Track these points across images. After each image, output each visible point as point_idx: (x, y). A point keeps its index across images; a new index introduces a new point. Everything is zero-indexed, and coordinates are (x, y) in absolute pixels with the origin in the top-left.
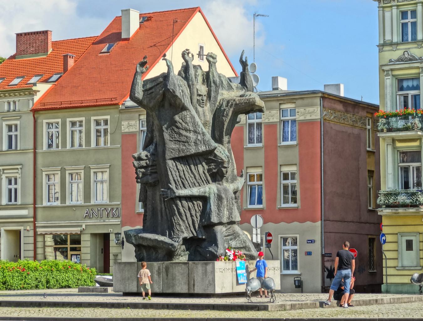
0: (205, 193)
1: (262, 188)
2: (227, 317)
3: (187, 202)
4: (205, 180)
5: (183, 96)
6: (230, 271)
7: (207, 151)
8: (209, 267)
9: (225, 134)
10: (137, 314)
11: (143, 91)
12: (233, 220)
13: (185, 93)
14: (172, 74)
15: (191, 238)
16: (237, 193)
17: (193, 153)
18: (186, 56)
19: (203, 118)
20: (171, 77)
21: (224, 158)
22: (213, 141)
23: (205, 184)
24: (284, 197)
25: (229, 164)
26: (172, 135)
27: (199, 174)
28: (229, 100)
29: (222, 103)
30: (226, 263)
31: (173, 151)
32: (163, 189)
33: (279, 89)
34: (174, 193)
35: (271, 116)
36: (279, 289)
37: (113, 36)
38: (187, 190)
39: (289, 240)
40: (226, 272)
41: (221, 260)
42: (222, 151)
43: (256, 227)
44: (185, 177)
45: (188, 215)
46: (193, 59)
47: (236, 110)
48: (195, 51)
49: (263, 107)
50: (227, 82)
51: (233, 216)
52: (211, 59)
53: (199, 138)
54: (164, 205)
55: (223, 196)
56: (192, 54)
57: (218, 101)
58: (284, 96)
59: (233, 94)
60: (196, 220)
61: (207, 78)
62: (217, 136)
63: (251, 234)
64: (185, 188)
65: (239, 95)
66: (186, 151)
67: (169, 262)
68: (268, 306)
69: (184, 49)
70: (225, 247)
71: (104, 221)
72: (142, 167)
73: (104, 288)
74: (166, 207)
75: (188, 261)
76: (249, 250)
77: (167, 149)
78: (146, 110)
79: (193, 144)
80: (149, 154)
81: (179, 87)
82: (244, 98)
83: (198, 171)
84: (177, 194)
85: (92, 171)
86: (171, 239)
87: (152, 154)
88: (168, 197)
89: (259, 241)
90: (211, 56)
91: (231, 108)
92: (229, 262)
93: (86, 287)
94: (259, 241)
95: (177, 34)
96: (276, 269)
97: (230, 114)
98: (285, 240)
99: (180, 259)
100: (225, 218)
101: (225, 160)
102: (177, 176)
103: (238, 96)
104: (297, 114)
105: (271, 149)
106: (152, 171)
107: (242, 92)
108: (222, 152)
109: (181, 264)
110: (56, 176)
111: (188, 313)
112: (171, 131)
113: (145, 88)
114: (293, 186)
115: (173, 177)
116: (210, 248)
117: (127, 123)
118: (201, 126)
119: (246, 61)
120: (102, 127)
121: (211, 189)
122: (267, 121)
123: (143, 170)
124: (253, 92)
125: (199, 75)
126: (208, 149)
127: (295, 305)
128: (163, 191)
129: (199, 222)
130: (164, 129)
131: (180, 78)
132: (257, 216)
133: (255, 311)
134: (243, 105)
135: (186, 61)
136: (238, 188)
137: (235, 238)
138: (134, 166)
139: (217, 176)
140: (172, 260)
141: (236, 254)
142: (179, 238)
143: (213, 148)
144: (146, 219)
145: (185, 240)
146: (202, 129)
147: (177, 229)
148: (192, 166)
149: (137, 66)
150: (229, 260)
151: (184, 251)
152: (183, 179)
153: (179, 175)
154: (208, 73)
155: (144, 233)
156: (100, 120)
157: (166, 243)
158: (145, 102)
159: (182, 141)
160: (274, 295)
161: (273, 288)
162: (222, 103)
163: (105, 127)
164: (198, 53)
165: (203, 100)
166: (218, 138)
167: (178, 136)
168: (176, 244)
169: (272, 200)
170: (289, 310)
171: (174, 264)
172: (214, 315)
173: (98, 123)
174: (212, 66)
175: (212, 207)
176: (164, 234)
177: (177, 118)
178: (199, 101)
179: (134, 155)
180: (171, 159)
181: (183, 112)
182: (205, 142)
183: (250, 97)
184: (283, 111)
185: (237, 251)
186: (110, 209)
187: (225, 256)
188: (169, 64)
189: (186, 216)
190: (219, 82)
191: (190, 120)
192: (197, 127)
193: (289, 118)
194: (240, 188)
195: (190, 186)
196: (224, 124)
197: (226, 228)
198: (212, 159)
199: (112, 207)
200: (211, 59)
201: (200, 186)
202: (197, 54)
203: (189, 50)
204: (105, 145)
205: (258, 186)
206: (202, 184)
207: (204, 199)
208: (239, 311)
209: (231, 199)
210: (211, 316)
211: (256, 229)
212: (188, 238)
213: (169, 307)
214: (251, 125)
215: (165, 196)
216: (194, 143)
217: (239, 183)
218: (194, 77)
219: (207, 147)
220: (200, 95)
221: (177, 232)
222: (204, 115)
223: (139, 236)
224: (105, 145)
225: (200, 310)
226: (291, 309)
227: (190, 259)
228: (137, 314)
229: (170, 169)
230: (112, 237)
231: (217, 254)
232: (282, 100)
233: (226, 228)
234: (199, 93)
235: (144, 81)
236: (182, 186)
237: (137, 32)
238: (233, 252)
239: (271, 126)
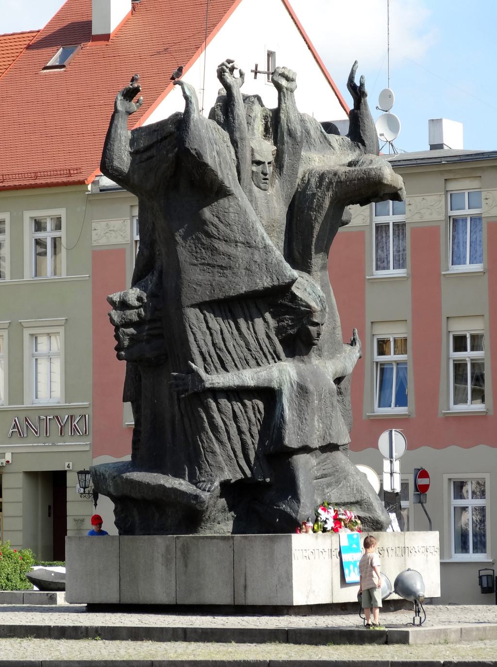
0: (271, 381)
1: (406, 368)
2: (315, 658)
3: (230, 401)
4: (269, 352)
5: (220, 164)
6: (327, 555)
7: (274, 287)
8: (279, 546)
9: (315, 248)
10: (114, 651)
11: (131, 153)
12: (334, 441)
13: (225, 158)
14: (195, 115)
15: (239, 482)
16: (343, 382)
17: (242, 291)
18: (227, 74)
19: (264, 214)
20: (192, 124)
21: (313, 304)
22: (288, 266)
23: (271, 361)
24: (455, 388)
25: (323, 316)
26: (196, 252)
27: (257, 339)
28: (323, 174)
29: (309, 180)
30: (317, 538)
31: (198, 288)
32: (175, 374)
33: (445, 146)
34: (201, 381)
35: (421, 207)
36: (437, 594)
37: (73, 32)
38: (229, 374)
39: (469, 488)
40: (317, 556)
41: (306, 532)
42: (309, 288)
43: (391, 456)
44: (225, 345)
45: (233, 430)
46: (243, 82)
47: (339, 194)
48: (244, 64)
49: (401, 189)
50: (319, 133)
51: (333, 434)
52: (282, 82)
53: (257, 257)
54: (179, 406)
55: (311, 387)
56: (240, 71)
57: (300, 175)
58: (454, 162)
59: (330, 159)
60: (249, 441)
61: (275, 125)
62: (297, 253)
63: (379, 472)
64: (227, 370)
65: (347, 162)
66: (227, 287)
67: (191, 535)
68: (407, 633)
69: (224, 60)
70: (316, 502)
71: (54, 445)
72: (128, 324)
73: (47, 594)
74: (183, 412)
75: (232, 533)
76: (369, 508)
77: (185, 282)
78: (137, 196)
79: (243, 271)
80: (144, 296)
81: (212, 146)
82: (357, 168)
83: (255, 333)
84: (207, 385)
85: (26, 333)
86: (195, 484)
87: (151, 296)
88: (187, 390)
89: (398, 489)
90: (283, 75)
91: (328, 190)
92: (325, 535)
93: (9, 591)
94: (398, 489)
95: (215, 25)
96: (431, 550)
97: (327, 203)
98: (459, 487)
99: (216, 529)
100: (315, 436)
101: (316, 307)
102: (206, 345)
103: (344, 165)
104: (484, 202)
105: (427, 284)
106: (151, 332)
107: (351, 157)
108: (308, 290)
109: (216, 540)
110: (53, 338)
111: (230, 650)
112: (194, 244)
113: (135, 147)
114: (477, 365)
115: (199, 347)
116: (281, 504)
117: (103, 224)
118: (261, 230)
119: (362, 85)
120: (47, 235)
121: (283, 373)
122: (416, 218)
123: (131, 330)
124: (378, 154)
125: (255, 117)
126: (276, 283)
127: (469, 631)
128: (175, 377)
129: (256, 446)
130: (179, 239)
131: (213, 124)
132: (393, 432)
133: (379, 644)
134: (354, 185)
135: (228, 87)
136: (345, 368)
137: (338, 482)
138: (112, 321)
139: (298, 340)
140: (195, 531)
141: (340, 516)
142: (212, 483)
143: (287, 281)
144: (139, 440)
145: (226, 486)
146: (263, 238)
147: (208, 462)
148: (242, 322)
149: (117, 98)
150: (325, 530)
151: (223, 511)
152: (220, 349)
153: (212, 340)
154: (276, 113)
155: (133, 471)
156: (45, 218)
157: (183, 493)
158: (136, 178)
159: (218, 266)
160: (421, 610)
161: (421, 593)
162: (309, 180)
163: (56, 234)
164: (254, 69)
165: (265, 174)
166: (298, 257)
167: (209, 253)
168: (205, 496)
169: (429, 398)
170: (456, 642)
171: (201, 541)
172: (287, 654)
173: (39, 226)
174: (284, 96)
175: (288, 413)
176: (178, 474)
177: (207, 213)
178: (257, 176)
179: (110, 296)
180: (193, 306)
181: (221, 201)
182: (269, 268)
183: (371, 167)
184: (453, 197)
185: (342, 511)
186: (67, 417)
187: (316, 521)
188: (188, 93)
189: (228, 432)
190: (302, 132)
191: (237, 218)
192: (252, 233)
193: (467, 212)
194: (350, 369)
195: (236, 365)
196: (313, 228)
197: (318, 460)
198: (286, 304)
199: (72, 413)
200: (284, 82)
201: (258, 365)
202: (252, 71)
203: (232, 62)
204: (55, 274)
205: (398, 364)
206: (264, 360)
207: (269, 395)
208: (345, 644)
209: (328, 395)
210: (279, 656)
211: (391, 462)
212: (232, 481)
213: (188, 636)
214: (381, 229)
215: (181, 388)
216: (246, 269)
217: (347, 360)
218: (244, 122)
219: (275, 278)
220: (259, 163)
221: (208, 469)
222: (268, 207)
223: (122, 477)
224: (55, 274)
225: (258, 643)
226: (459, 641)
227: (234, 532)
228: (114, 651)
229: (191, 328)
230: (72, 480)
231: (298, 518)
232: (450, 171)
233: (318, 460)
234: (258, 158)
235: (133, 132)
236: (219, 366)
237: (125, 23)
238: (333, 514)
239: (427, 235)
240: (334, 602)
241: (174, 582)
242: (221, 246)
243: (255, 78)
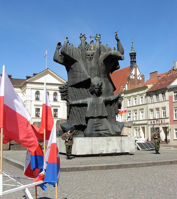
53: (82, 75)
240: (93, 154)
242: (75, 73)
243: (91, 38)
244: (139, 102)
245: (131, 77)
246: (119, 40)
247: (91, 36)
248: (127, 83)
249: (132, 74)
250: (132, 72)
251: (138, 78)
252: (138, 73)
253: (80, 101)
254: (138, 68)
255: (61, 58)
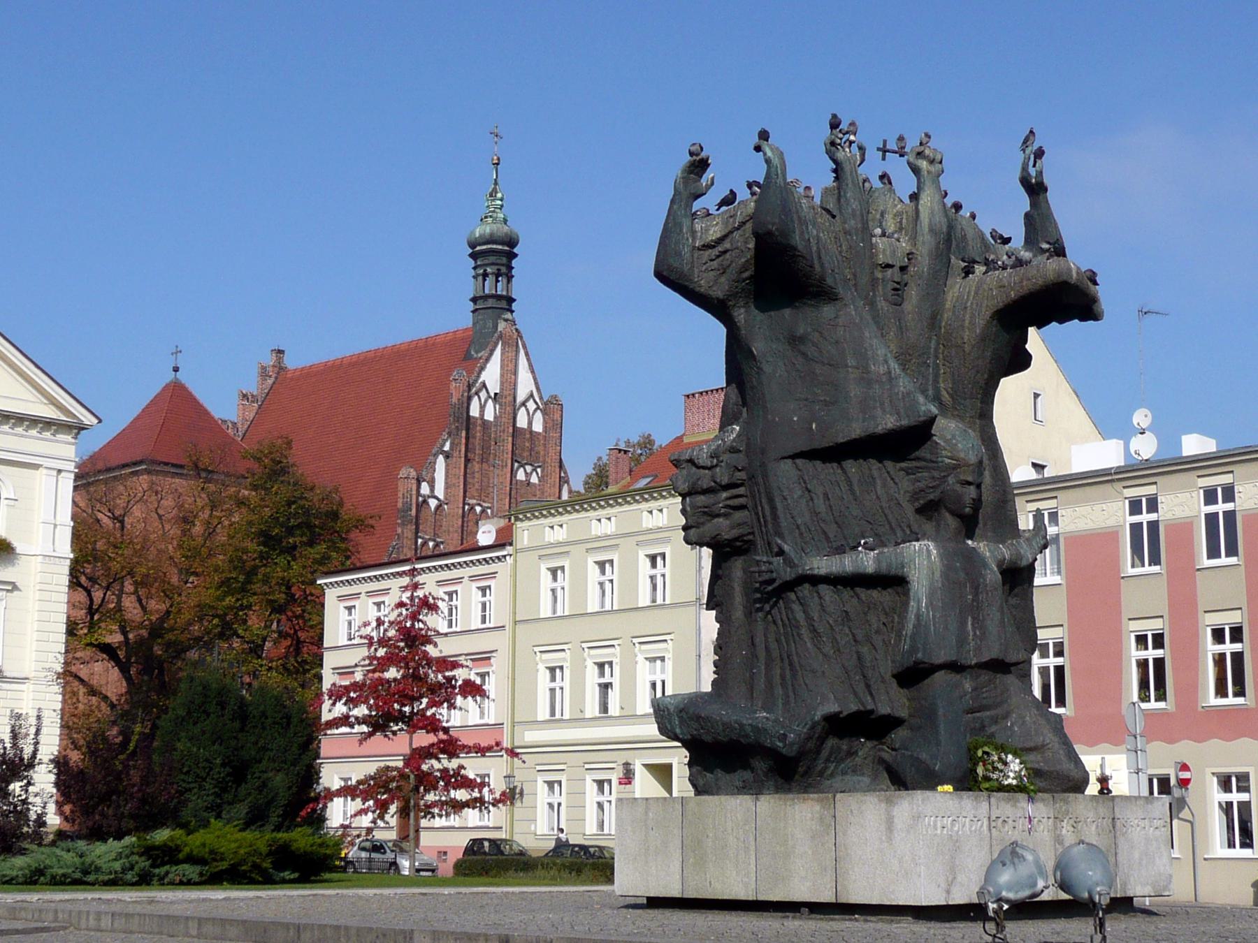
169: (1191, 689)
202: (879, 149)
241: (753, 862)
243: (884, 159)
244: (631, 586)
245: (474, 411)
246: (1046, 190)
247: (885, 142)
248: (447, 448)
249: (484, 385)
250: (482, 368)
251: (522, 422)
252: (525, 385)
253: (867, 561)
254: (527, 354)
255: (715, 264)
